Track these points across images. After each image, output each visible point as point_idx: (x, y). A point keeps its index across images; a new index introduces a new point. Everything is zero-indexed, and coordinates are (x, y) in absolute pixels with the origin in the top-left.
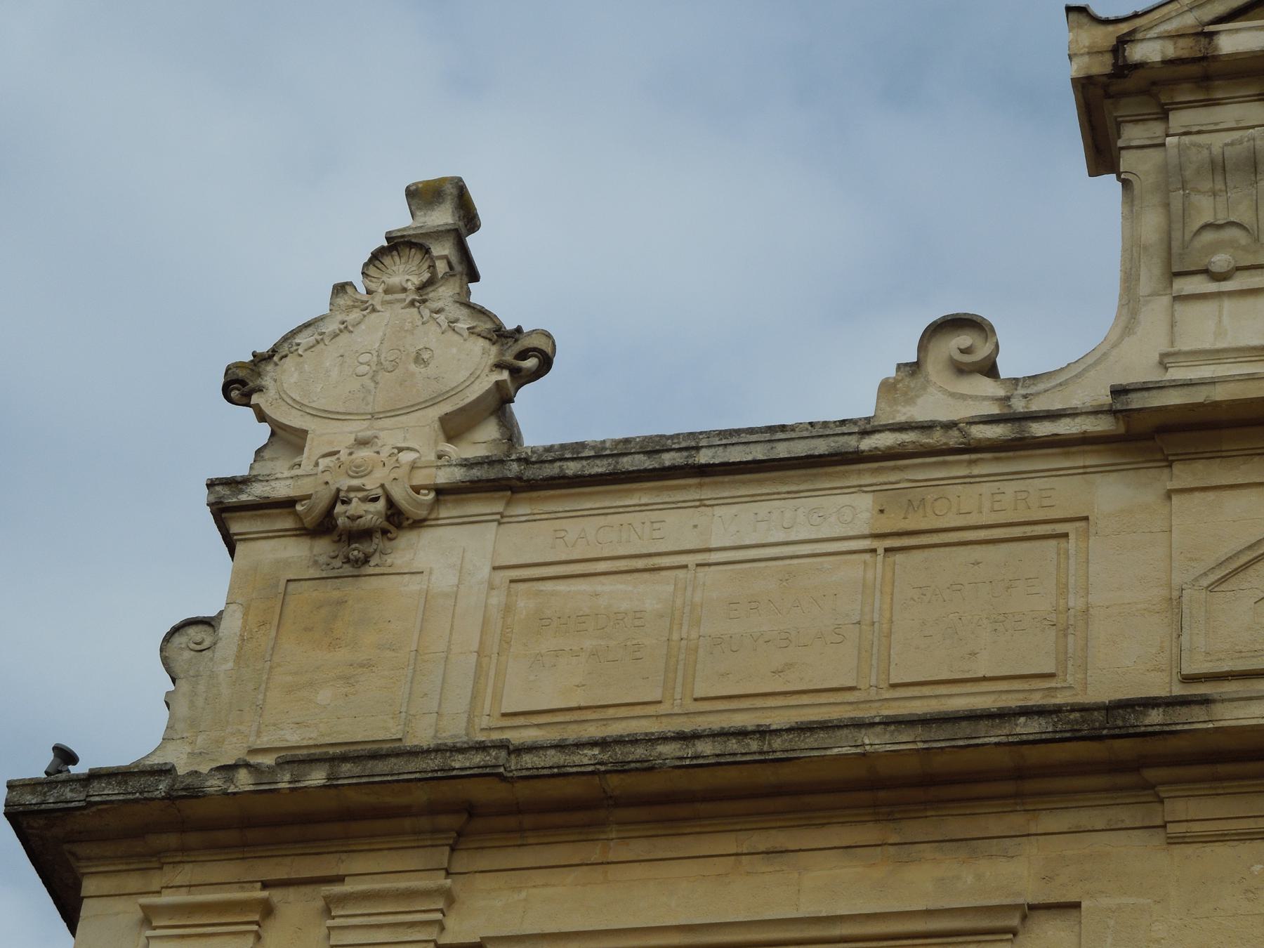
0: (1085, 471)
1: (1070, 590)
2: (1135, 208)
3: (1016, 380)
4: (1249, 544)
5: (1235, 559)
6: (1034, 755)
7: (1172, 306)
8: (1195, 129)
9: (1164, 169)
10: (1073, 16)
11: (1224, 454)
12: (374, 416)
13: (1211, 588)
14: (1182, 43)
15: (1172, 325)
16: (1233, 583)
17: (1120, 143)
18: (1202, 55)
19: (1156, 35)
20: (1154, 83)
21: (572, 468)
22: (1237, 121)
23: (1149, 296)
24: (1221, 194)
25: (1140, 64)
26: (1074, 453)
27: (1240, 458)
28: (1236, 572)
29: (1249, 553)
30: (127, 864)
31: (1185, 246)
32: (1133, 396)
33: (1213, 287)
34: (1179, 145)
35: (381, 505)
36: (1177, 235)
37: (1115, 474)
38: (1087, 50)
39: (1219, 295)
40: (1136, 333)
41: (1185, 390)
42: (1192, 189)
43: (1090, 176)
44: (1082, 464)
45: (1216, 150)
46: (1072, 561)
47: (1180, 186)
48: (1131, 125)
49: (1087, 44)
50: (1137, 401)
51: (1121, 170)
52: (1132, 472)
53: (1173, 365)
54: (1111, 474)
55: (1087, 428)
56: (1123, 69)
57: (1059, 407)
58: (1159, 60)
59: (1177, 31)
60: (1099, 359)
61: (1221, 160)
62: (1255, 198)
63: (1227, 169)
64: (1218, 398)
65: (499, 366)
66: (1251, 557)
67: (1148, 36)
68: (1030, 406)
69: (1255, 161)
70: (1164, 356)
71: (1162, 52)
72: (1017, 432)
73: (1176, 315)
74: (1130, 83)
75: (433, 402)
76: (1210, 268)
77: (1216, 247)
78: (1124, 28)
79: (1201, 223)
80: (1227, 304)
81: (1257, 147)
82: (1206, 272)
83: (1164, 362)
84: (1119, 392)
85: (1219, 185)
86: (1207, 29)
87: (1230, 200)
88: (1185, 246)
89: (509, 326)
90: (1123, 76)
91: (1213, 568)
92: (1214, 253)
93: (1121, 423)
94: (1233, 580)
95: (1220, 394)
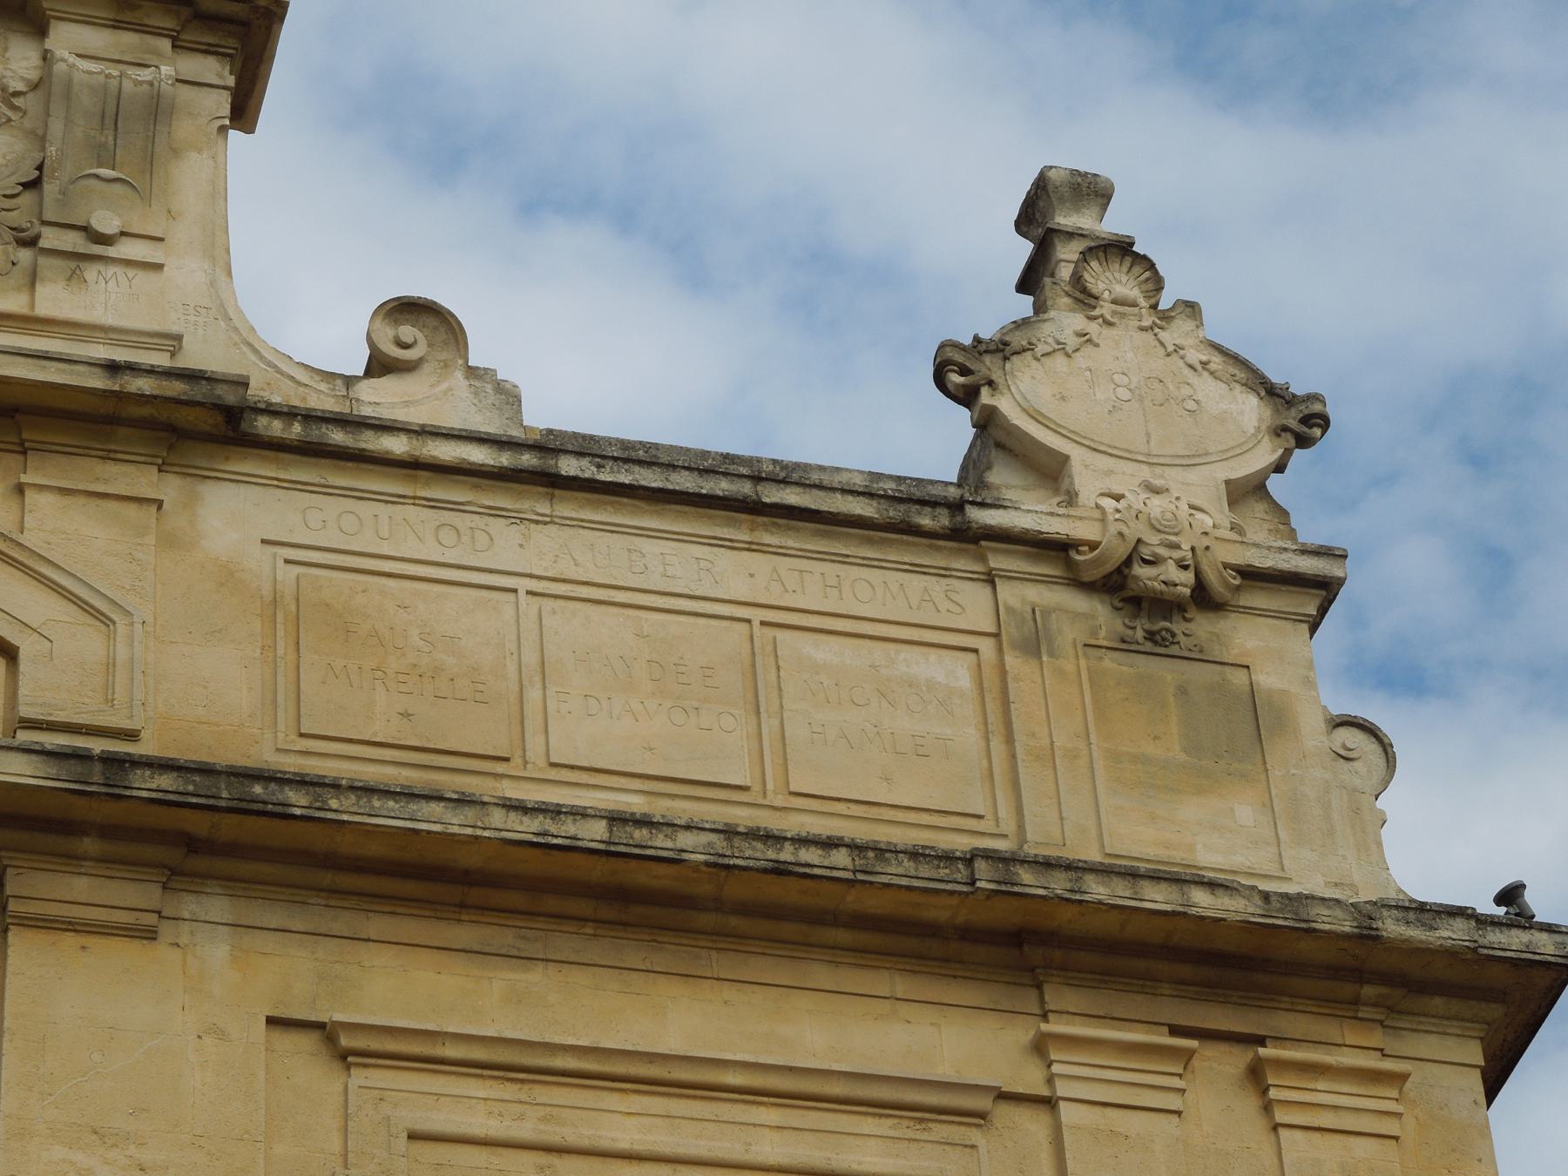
30: (713, 941)
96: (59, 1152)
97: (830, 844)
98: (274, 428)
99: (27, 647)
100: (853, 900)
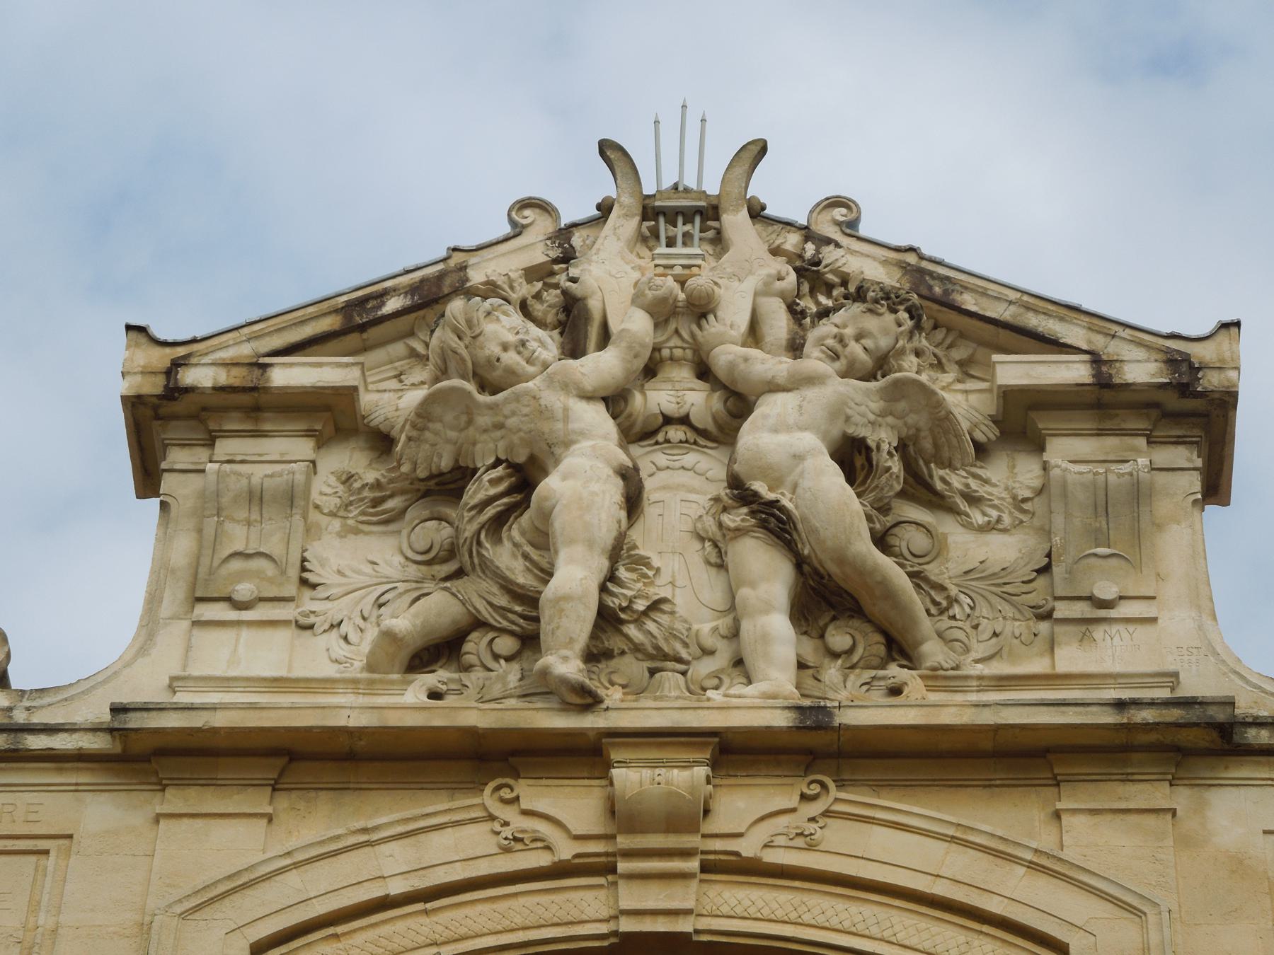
0: (77, 788)
1: (42, 908)
2: (169, 531)
3: (23, 692)
4: (229, 874)
5: (213, 888)
7: (190, 631)
8: (239, 458)
9: (202, 495)
10: (133, 334)
11: (219, 782)
13: (184, 916)
14: (236, 371)
15: (188, 649)
16: (206, 913)
17: (164, 466)
18: (253, 385)
19: (210, 362)
20: (204, 409)
22: (282, 454)
23: (169, 619)
24: (256, 524)
25: (191, 388)
26: (67, 769)
27: (235, 787)
28: (212, 901)
29: (228, 883)
31: (211, 572)
32: (131, 715)
33: (233, 615)
34: (219, 471)
36: (205, 561)
37: (107, 794)
38: (140, 369)
39: (238, 623)
40: (150, 654)
41: (187, 714)
42: (227, 517)
43: (137, 498)
44: (74, 781)
45: (256, 480)
46: (49, 878)
47: (215, 512)
48: (176, 448)
49: (142, 364)
50: (134, 721)
51: (161, 492)
52: (124, 793)
53: (181, 689)
54: (103, 794)
55: (84, 744)
56: (174, 392)
57: (61, 721)
58: (210, 385)
59: (231, 359)
60: (110, 676)
61: (259, 491)
62: (287, 531)
63: (264, 500)
64: (217, 725)
66: (229, 888)
67: (202, 362)
68: (31, 718)
69: (292, 495)
70: (174, 679)
71: (215, 379)
72: (11, 743)
73: (193, 640)
74: (178, 407)
76: (233, 596)
77: (242, 576)
78: (181, 351)
79: (231, 551)
80: (245, 633)
81: (296, 481)
82: (228, 599)
83: (174, 684)
84: (117, 710)
85: (255, 516)
86: (262, 360)
87: (264, 531)
88: (211, 572)
90: (172, 399)
91: (189, 896)
92: (239, 582)
93: (118, 741)
94: (206, 909)
95: (220, 720)
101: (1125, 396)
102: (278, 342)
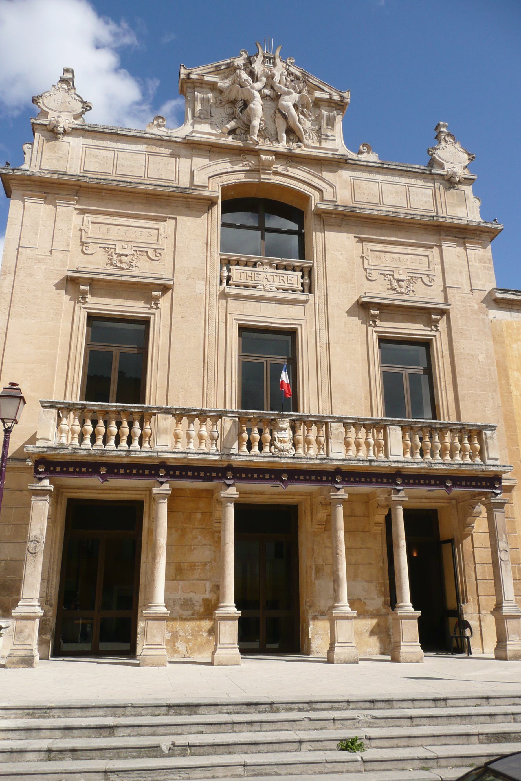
6: (172, 194)
12: (61, 112)
21: (96, 129)
35: (63, 129)
65: (83, 108)
75: (72, 112)
89: (85, 100)
95: (202, 140)
96: (333, 252)
97: (418, 215)
98: (350, 161)
99: (324, 190)
100: (419, 222)
101: (333, 101)
102: (206, 71)
